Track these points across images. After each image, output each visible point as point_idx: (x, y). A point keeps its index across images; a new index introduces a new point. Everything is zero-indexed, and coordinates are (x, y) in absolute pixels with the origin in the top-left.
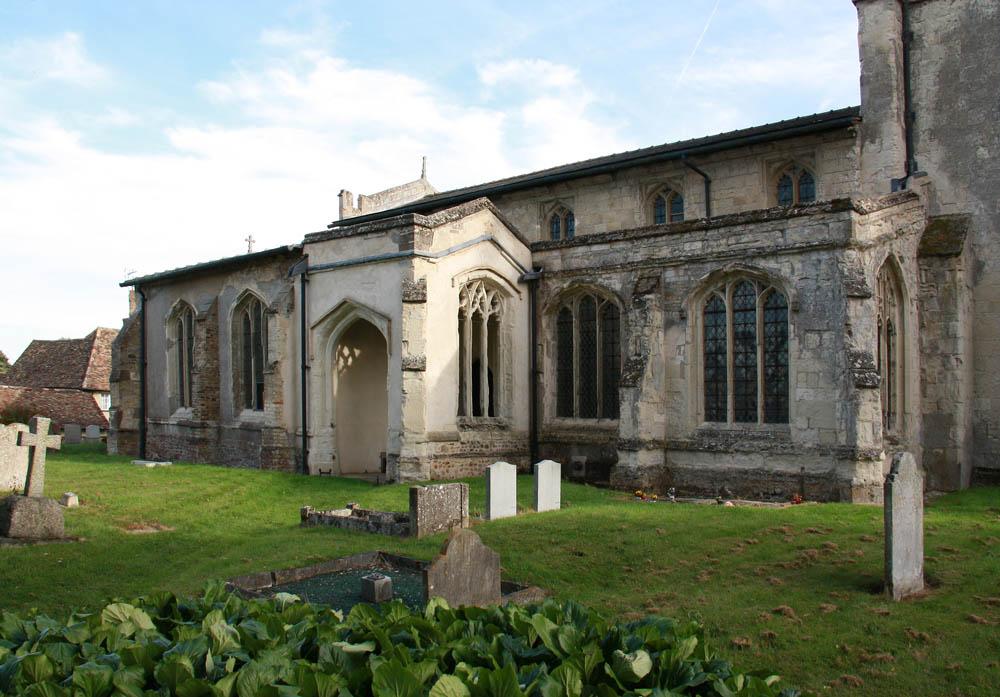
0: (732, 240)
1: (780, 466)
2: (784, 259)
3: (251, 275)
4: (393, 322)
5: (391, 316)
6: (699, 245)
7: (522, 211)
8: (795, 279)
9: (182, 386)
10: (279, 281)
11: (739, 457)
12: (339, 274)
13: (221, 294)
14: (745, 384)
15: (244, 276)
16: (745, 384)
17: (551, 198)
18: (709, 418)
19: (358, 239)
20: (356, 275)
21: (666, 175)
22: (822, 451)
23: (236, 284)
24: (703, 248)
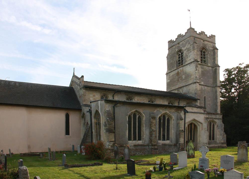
0: (211, 116)
1: (216, 145)
2: (216, 120)
3: (166, 109)
4: (203, 124)
5: (203, 123)
6: (208, 116)
7: (144, 99)
8: (217, 122)
9: (194, 136)
10: (176, 112)
11: (212, 145)
12: (192, 114)
13: (155, 112)
14: (164, 136)
15: (164, 109)
16: (164, 136)
17: (150, 98)
18: (210, 140)
19: (196, 108)
20: (196, 115)
21: (172, 100)
22: (220, 143)
23: (161, 111)
24: (208, 117)
